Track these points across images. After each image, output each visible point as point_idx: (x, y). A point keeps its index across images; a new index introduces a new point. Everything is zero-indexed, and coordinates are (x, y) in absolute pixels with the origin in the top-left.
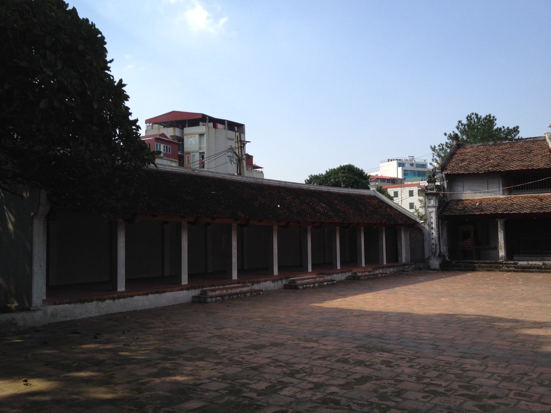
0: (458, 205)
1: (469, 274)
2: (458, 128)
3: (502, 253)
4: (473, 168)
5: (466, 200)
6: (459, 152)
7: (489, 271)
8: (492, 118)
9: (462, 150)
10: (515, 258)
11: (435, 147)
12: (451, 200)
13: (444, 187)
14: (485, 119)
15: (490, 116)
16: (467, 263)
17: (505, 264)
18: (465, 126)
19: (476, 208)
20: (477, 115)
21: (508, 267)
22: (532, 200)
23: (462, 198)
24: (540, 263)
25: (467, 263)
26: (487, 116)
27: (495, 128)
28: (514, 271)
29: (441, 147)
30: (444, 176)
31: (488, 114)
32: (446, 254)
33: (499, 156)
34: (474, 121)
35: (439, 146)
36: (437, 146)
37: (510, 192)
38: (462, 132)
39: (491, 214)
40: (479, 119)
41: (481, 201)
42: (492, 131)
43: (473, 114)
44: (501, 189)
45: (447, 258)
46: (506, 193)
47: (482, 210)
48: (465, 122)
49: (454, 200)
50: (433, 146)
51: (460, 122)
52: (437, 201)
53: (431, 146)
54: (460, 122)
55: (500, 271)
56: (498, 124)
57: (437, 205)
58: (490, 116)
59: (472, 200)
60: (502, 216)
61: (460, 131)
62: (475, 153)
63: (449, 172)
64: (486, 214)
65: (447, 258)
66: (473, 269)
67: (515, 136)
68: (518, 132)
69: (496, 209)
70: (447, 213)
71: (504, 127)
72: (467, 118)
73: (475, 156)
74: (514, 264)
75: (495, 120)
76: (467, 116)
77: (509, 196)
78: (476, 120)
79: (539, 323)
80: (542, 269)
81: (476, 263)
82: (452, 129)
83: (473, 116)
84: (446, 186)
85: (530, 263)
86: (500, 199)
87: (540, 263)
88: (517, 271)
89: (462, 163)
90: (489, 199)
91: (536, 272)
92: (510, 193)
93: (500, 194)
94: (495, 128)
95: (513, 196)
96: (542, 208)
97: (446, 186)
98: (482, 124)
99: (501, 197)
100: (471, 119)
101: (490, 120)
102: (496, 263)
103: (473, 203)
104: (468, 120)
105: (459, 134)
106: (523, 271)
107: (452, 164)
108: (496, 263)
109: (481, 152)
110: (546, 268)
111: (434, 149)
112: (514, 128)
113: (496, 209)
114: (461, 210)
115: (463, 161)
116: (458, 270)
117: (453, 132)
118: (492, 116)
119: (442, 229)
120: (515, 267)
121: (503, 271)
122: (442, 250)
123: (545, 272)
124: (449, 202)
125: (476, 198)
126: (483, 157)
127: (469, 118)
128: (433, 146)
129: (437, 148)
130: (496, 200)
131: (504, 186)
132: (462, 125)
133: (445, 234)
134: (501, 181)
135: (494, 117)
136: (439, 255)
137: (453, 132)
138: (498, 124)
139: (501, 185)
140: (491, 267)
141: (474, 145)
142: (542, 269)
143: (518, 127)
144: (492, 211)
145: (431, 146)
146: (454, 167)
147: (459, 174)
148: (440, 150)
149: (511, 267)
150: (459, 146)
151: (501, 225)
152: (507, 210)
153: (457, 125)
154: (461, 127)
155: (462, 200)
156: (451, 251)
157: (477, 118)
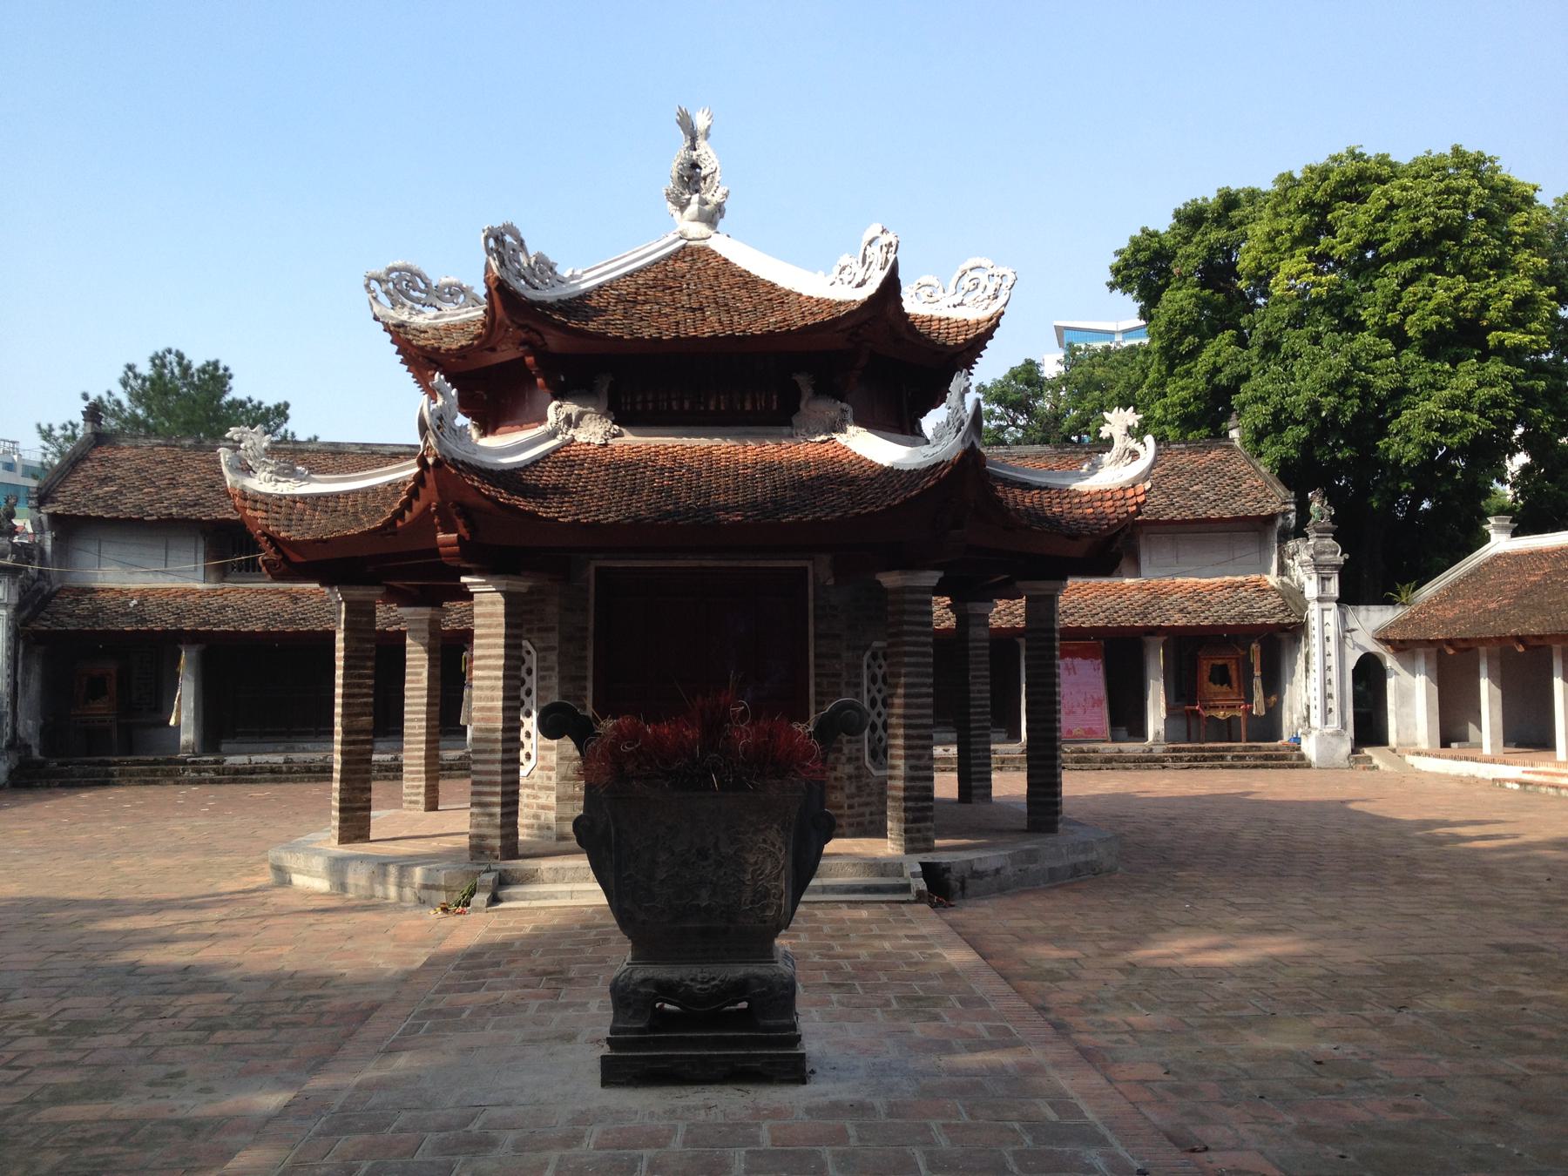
0: (78, 601)
1: (84, 796)
2: (125, 383)
3: (188, 736)
4: (128, 505)
5: (103, 590)
6: (96, 454)
7: (147, 783)
8: (221, 372)
9: (106, 452)
10: (224, 747)
11: (51, 428)
12: (62, 589)
13: (42, 551)
14: (203, 370)
15: (216, 365)
16: (90, 764)
17: (194, 763)
18: (144, 380)
19: (126, 614)
20: (180, 356)
21: (199, 772)
22: (274, 598)
23: (94, 585)
24: (278, 759)
25: (90, 764)
26: (208, 364)
27: (228, 398)
28: (212, 782)
29: (69, 433)
30: (45, 518)
31: (212, 359)
32: (34, 742)
33: (203, 479)
34: (172, 372)
35: (64, 428)
36: (56, 426)
37: (223, 573)
38: (136, 397)
39: (166, 631)
40: (186, 369)
41: (144, 595)
42: (220, 407)
43: (170, 352)
44: (201, 565)
45: (36, 753)
46: (212, 578)
47: (144, 621)
48: (145, 369)
49: (71, 590)
50: (45, 427)
51: (130, 368)
52: (15, 590)
53: (39, 426)
54: (130, 368)
55: (177, 783)
56: (238, 390)
57: (15, 600)
58: (216, 365)
59: (120, 592)
60: (193, 637)
61: (131, 394)
62: (143, 464)
63: (60, 509)
64: (151, 631)
65: (36, 753)
66: (103, 780)
67: (278, 426)
68: (286, 419)
69: (180, 617)
70: (42, 626)
71: (250, 400)
72: (152, 360)
73: (140, 475)
74: (216, 762)
75: (230, 377)
76: (151, 354)
77: (217, 586)
78: (177, 371)
79: (160, 902)
80: (281, 772)
81: (115, 764)
82: (107, 385)
83: (171, 358)
84: (48, 547)
85: (256, 758)
86: (193, 592)
87: (278, 759)
88: (220, 782)
89: (100, 487)
90: (165, 589)
91: (266, 781)
92: (221, 580)
93: (198, 581)
94: (228, 398)
95: (227, 585)
96: (292, 621)
97: (48, 547)
98: (192, 383)
99: (200, 586)
100: (164, 366)
101: (216, 377)
102: (169, 762)
103: (122, 599)
104: (154, 365)
105: (126, 403)
106: (234, 781)
107: (73, 487)
108: (169, 762)
109: (157, 463)
110: (290, 771)
111: (1112, 286)
112: (277, 407)
113: (180, 617)
114: (84, 617)
115: (104, 481)
116: (61, 785)
117: (110, 393)
118: (221, 365)
119: (26, 670)
120: (217, 772)
121: (183, 783)
122: (21, 730)
123: (287, 780)
124: (54, 595)
125: (134, 586)
126: (161, 476)
127: (158, 361)
128: (45, 427)
129: (57, 433)
130: (185, 593)
131: (207, 558)
132: (136, 377)
133: (34, 685)
134: (201, 545)
135: (226, 369)
136: (11, 746)
137: (110, 393)
138: (238, 390)
139: (201, 556)
140: (153, 773)
141: (140, 442)
142: (281, 772)
143: (287, 405)
144: (169, 622)
145: (39, 426)
146: (75, 498)
147: (87, 518)
148: (67, 439)
149: (205, 771)
150: (99, 438)
151: (188, 660)
152: (208, 623)
153: (121, 375)
154: (132, 382)
155: (93, 590)
156: (52, 734)
157: (180, 364)
